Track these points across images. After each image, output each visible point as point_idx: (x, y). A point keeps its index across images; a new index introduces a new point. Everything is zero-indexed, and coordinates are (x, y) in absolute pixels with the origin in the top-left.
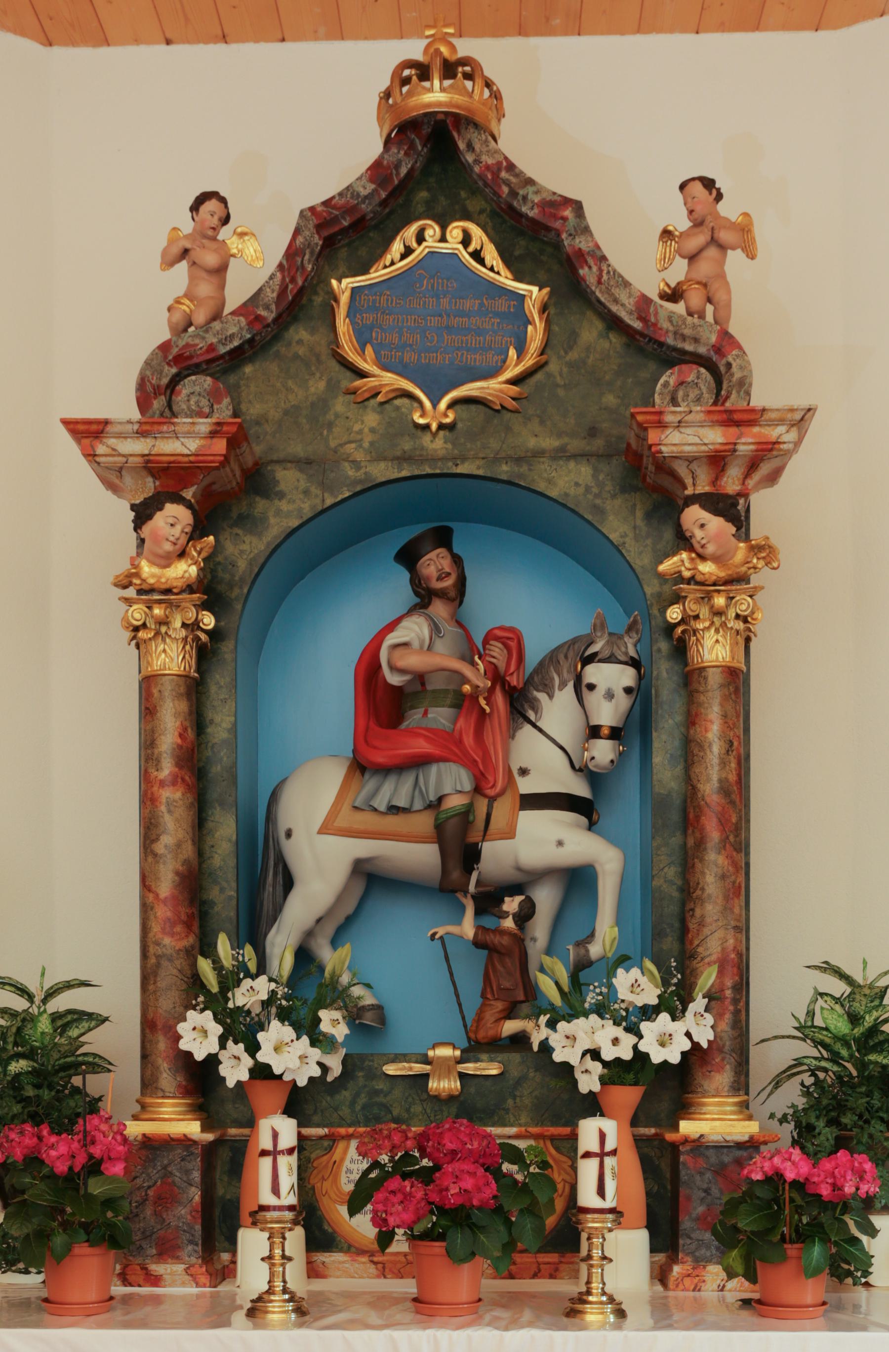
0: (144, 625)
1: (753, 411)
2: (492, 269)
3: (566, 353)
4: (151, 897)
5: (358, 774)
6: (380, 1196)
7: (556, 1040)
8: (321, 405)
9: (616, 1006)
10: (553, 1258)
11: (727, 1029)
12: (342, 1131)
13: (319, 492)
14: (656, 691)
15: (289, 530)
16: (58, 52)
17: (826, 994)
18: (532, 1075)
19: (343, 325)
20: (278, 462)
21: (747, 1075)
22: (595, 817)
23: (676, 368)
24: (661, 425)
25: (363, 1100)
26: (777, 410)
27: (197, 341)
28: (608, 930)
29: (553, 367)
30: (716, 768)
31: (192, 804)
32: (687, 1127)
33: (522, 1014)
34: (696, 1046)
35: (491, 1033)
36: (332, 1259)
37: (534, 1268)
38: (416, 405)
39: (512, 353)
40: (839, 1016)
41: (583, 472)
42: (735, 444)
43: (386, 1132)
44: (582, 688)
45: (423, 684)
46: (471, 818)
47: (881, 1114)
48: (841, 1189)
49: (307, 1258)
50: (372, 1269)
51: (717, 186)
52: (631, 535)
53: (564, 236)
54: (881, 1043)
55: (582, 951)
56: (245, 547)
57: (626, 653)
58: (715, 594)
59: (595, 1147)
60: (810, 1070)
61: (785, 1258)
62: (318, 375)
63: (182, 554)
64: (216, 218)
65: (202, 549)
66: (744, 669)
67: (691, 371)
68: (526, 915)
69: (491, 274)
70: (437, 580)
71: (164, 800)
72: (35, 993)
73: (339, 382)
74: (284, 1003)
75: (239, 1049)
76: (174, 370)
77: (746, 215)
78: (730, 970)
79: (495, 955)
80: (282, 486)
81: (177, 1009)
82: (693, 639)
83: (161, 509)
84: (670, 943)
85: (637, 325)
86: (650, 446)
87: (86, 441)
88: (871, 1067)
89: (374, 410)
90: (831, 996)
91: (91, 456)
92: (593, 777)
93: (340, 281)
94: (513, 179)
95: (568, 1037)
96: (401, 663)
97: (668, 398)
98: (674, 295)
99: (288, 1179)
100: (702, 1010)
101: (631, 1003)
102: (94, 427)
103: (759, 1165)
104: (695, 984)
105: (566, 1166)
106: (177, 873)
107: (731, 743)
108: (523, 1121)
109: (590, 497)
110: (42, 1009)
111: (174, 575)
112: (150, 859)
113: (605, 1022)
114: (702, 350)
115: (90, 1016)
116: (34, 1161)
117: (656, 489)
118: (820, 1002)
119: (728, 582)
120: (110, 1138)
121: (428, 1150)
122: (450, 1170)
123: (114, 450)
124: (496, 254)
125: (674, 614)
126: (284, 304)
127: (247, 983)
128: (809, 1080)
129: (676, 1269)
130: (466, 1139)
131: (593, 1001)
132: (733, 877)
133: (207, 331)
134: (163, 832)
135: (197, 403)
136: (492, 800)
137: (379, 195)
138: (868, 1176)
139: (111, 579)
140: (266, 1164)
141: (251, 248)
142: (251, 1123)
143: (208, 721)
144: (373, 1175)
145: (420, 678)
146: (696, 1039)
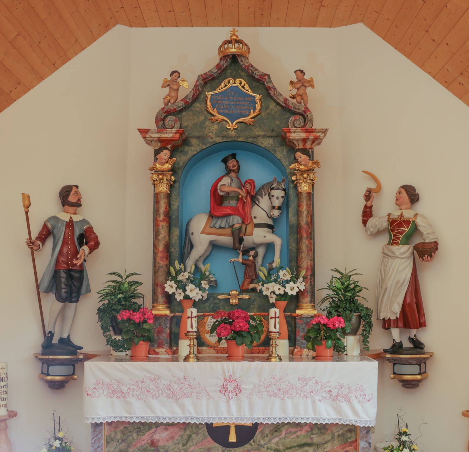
0: (157, 180)
1: (313, 129)
2: (247, 90)
3: (266, 111)
4: (157, 251)
5: (211, 218)
6: (218, 328)
7: (264, 289)
8: (203, 123)
9: (280, 280)
10: (263, 348)
11: (309, 286)
12: (207, 314)
13: (202, 145)
14: (290, 197)
15: (194, 155)
16: (134, 29)
17: (336, 277)
18: (257, 298)
19: (209, 103)
20: (191, 137)
21: (314, 299)
22: (274, 229)
23: (294, 116)
24: (290, 132)
25: (212, 305)
26: (319, 129)
27: (171, 107)
28: (277, 260)
29: (263, 114)
30: (305, 218)
31: (168, 226)
32: (298, 312)
33: (255, 282)
34: (300, 290)
35: (246, 287)
36: (204, 349)
37: (258, 351)
38: (227, 123)
39: (252, 111)
40: (339, 283)
41: (271, 141)
42: (309, 137)
43: (220, 312)
44: (270, 196)
45: (228, 194)
46: (241, 230)
47: (349, 309)
48: (335, 325)
49: (197, 348)
50: (214, 352)
51: (304, 72)
52: (283, 157)
53: (265, 83)
54: (349, 290)
55: (271, 266)
56: (182, 159)
57: (282, 187)
58: (304, 174)
59: (273, 316)
60: (331, 298)
61: (322, 344)
62: (202, 115)
63: (167, 162)
64: (177, 77)
65: (172, 161)
66: (312, 192)
67: (298, 117)
68: (255, 256)
69: (247, 92)
70: (232, 167)
71: (161, 225)
72: (123, 277)
73: (207, 117)
74: (192, 279)
75: (181, 291)
76: (165, 114)
77: (311, 78)
78: (309, 271)
79: (248, 267)
80: (192, 143)
81: (164, 281)
82: (299, 185)
83: (162, 151)
84: (294, 263)
85: (284, 105)
86: (287, 137)
87: (144, 134)
88: (347, 296)
89: (216, 124)
90: (337, 278)
91: (144, 138)
92: (274, 220)
93: (208, 93)
94: (252, 69)
95: (267, 288)
96: (223, 190)
97: (292, 123)
98: (293, 97)
99: (195, 325)
100: (302, 281)
101: (283, 279)
102: (146, 131)
103: (315, 320)
104: (300, 274)
105: (266, 323)
106: (164, 245)
107: (309, 212)
108: (255, 311)
109: (272, 147)
110: (125, 281)
111: (165, 167)
112: (157, 241)
113: (276, 284)
114: (301, 112)
115: (138, 283)
116: (129, 320)
117: (289, 146)
118: (334, 279)
119: (307, 170)
120: (149, 313)
121: (231, 317)
122: (237, 321)
123: (151, 136)
124: (248, 87)
125: (294, 178)
126: (194, 98)
127: (182, 274)
128: (331, 300)
129: (296, 350)
130: (241, 314)
131: (273, 279)
132: (309, 247)
133: (174, 105)
134: (161, 234)
135: (171, 123)
136: (247, 225)
137: (218, 72)
138: (342, 323)
139: (148, 168)
140: (189, 320)
141: (185, 85)
142: (182, 311)
143: (172, 204)
144: (216, 324)
145: (228, 193)
146: (300, 289)
